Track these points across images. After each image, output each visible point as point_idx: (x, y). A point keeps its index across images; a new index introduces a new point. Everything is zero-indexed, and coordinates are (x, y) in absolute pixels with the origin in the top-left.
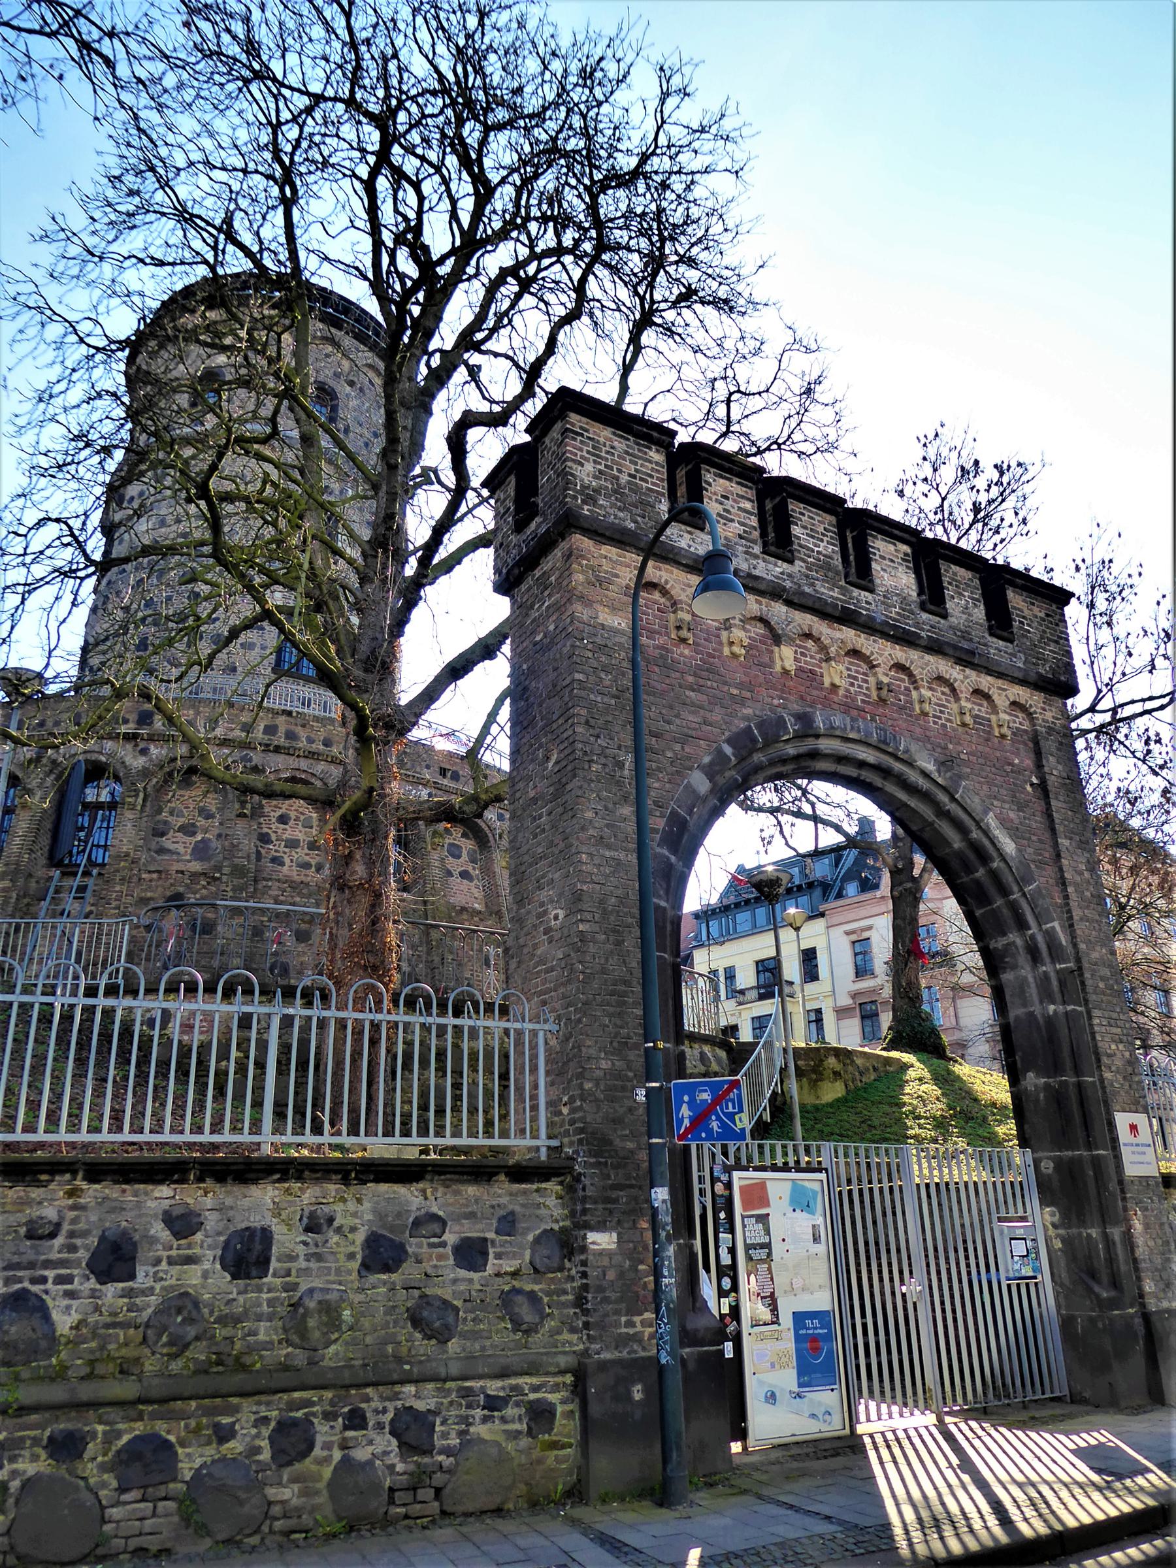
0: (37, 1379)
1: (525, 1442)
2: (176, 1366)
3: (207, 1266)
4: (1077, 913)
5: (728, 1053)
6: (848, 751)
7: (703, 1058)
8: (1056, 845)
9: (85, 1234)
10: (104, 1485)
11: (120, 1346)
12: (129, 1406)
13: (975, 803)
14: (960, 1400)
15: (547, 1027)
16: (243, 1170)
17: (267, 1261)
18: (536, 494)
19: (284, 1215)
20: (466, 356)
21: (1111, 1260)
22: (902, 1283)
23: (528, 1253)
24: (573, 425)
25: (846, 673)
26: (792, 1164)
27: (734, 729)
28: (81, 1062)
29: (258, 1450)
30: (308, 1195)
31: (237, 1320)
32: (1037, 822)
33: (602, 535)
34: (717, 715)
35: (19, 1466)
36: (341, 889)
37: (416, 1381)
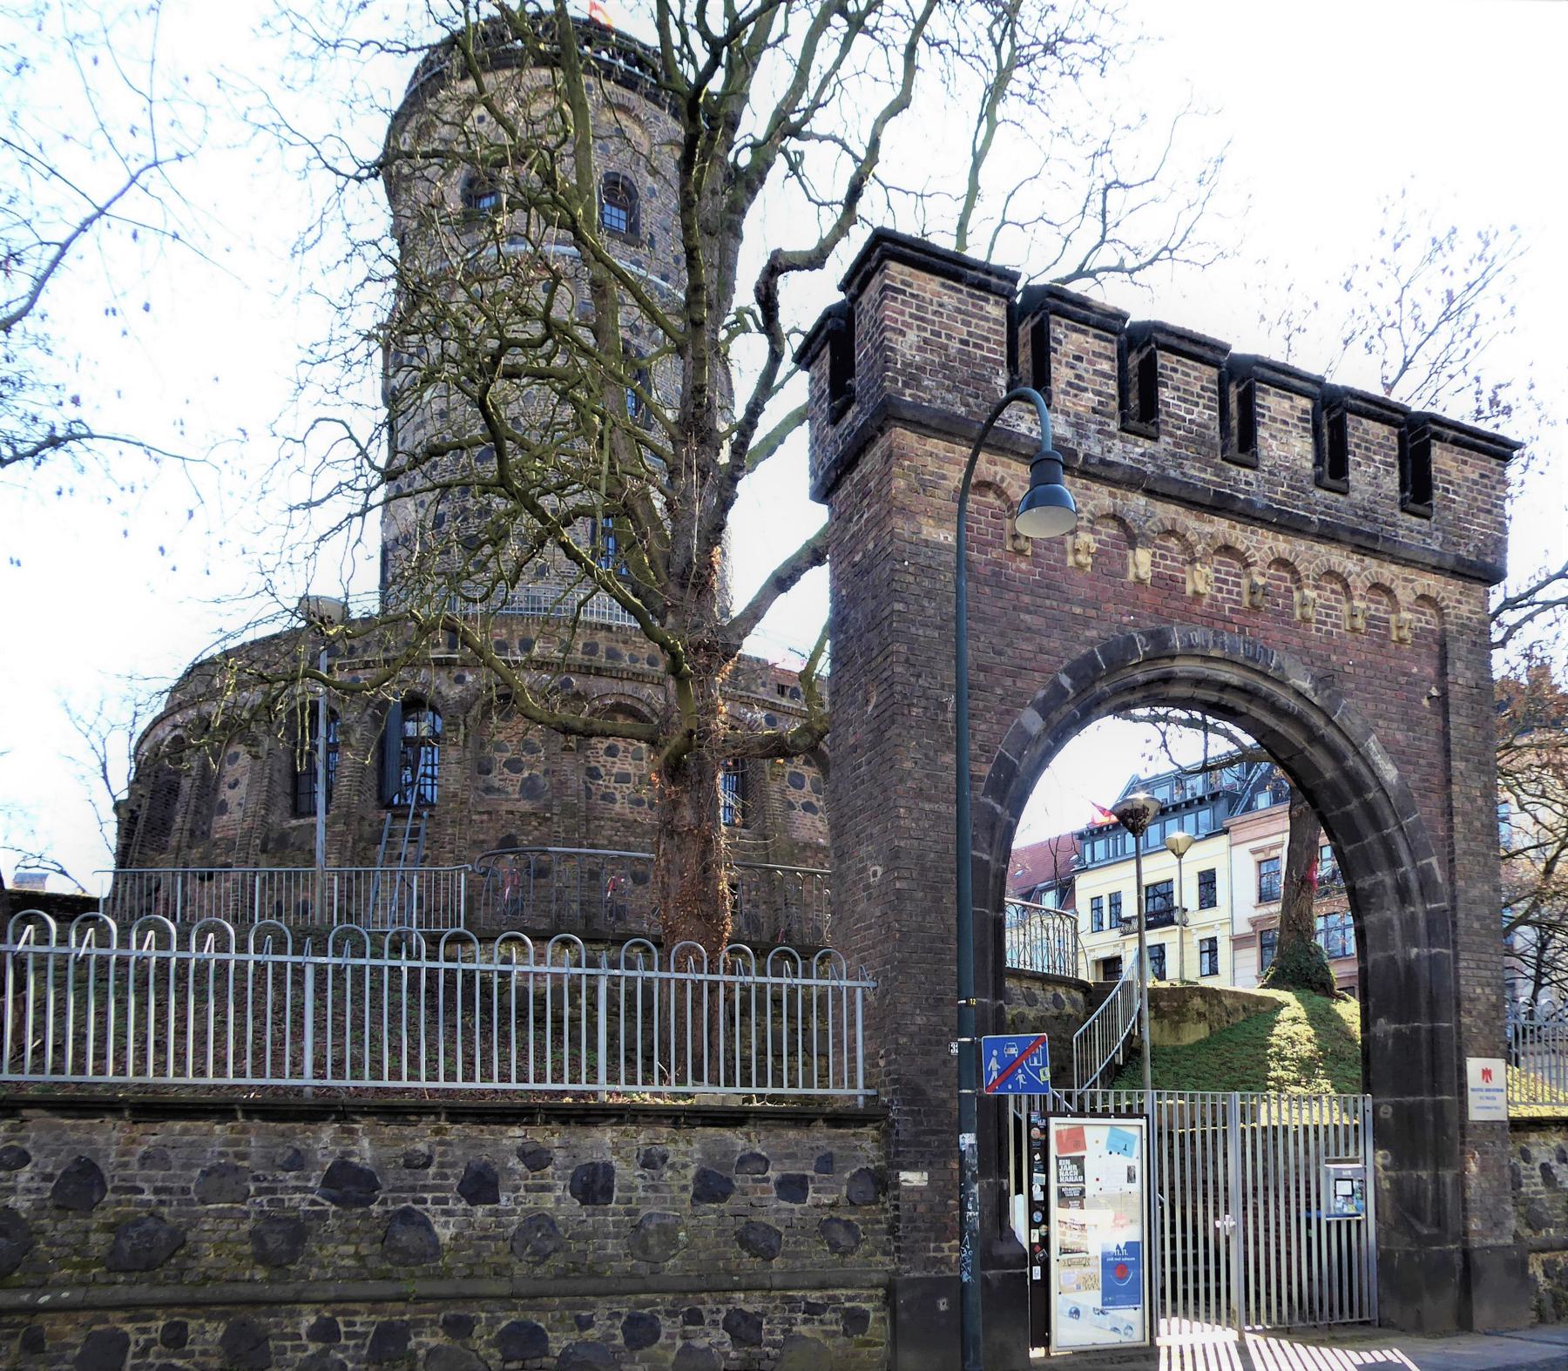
0: (427, 1276)
1: (841, 1340)
2: (539, 1271)
3: (559, 1193)
4: (1460, 847)
5: (1085, 994)
6: (1207, 672)
7: (1057, 1000)
8: (1448, 767)
9: (453, 1165)
10: (491, 1356)
11: (493, 1254)
12: (508, 1300)
13: (1354, 725)
14: (1263, 1321)
15: (864, 984)
16: (587, 1115)
17: (611, 1191)
18: (852, 375)
19: (623, 1153)
20: (783, 144)
21: (1439, 1200)
22: (1216, 1216)
23: (844, 1190)
24: (893, 279)
25: (1212, 576)
26: (1112, 1110)
27: (1074, 656)
28: (432, 1008)
29: (614, 1337)
30: (644, 1137)
31: (587, 1238)
32: (1429, 744)
33: (927, 426)
34: (1054, 643)
35: (423, 1339)
36: (671, 834)
37: (745, 1290)
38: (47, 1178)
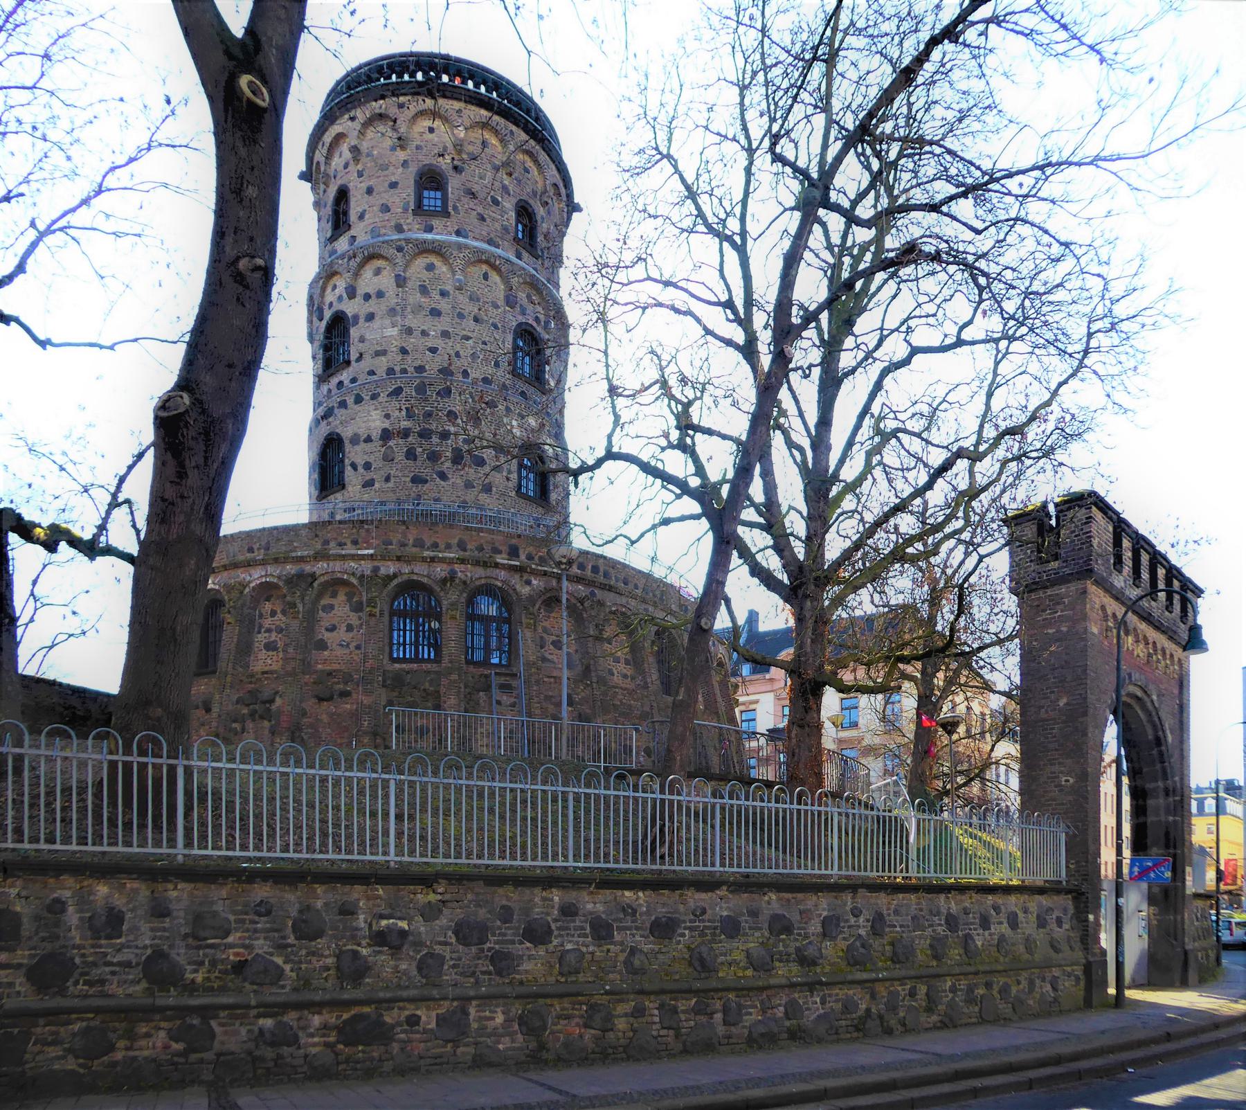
21: (1175, 927)
38: (868, 921)
